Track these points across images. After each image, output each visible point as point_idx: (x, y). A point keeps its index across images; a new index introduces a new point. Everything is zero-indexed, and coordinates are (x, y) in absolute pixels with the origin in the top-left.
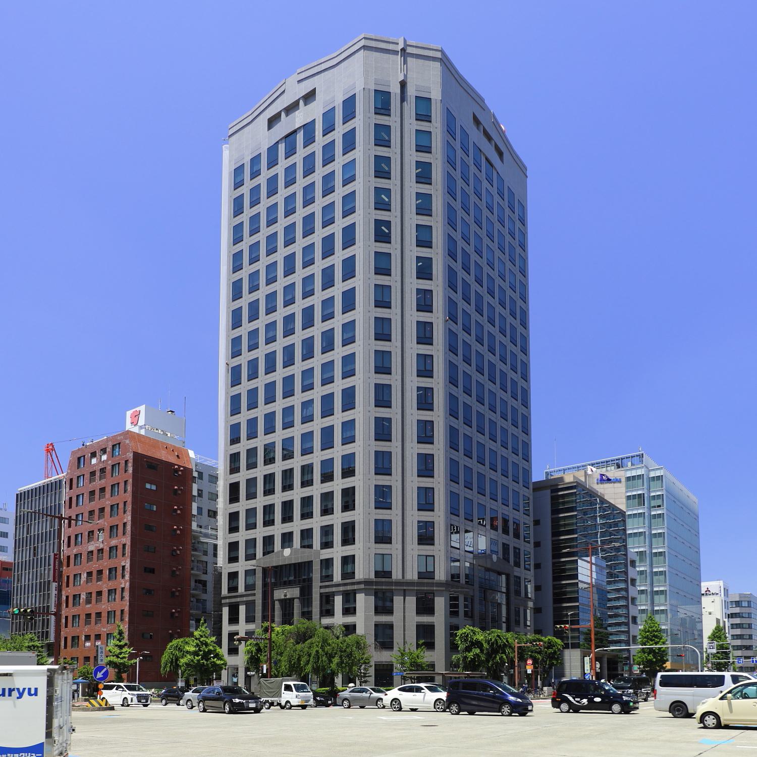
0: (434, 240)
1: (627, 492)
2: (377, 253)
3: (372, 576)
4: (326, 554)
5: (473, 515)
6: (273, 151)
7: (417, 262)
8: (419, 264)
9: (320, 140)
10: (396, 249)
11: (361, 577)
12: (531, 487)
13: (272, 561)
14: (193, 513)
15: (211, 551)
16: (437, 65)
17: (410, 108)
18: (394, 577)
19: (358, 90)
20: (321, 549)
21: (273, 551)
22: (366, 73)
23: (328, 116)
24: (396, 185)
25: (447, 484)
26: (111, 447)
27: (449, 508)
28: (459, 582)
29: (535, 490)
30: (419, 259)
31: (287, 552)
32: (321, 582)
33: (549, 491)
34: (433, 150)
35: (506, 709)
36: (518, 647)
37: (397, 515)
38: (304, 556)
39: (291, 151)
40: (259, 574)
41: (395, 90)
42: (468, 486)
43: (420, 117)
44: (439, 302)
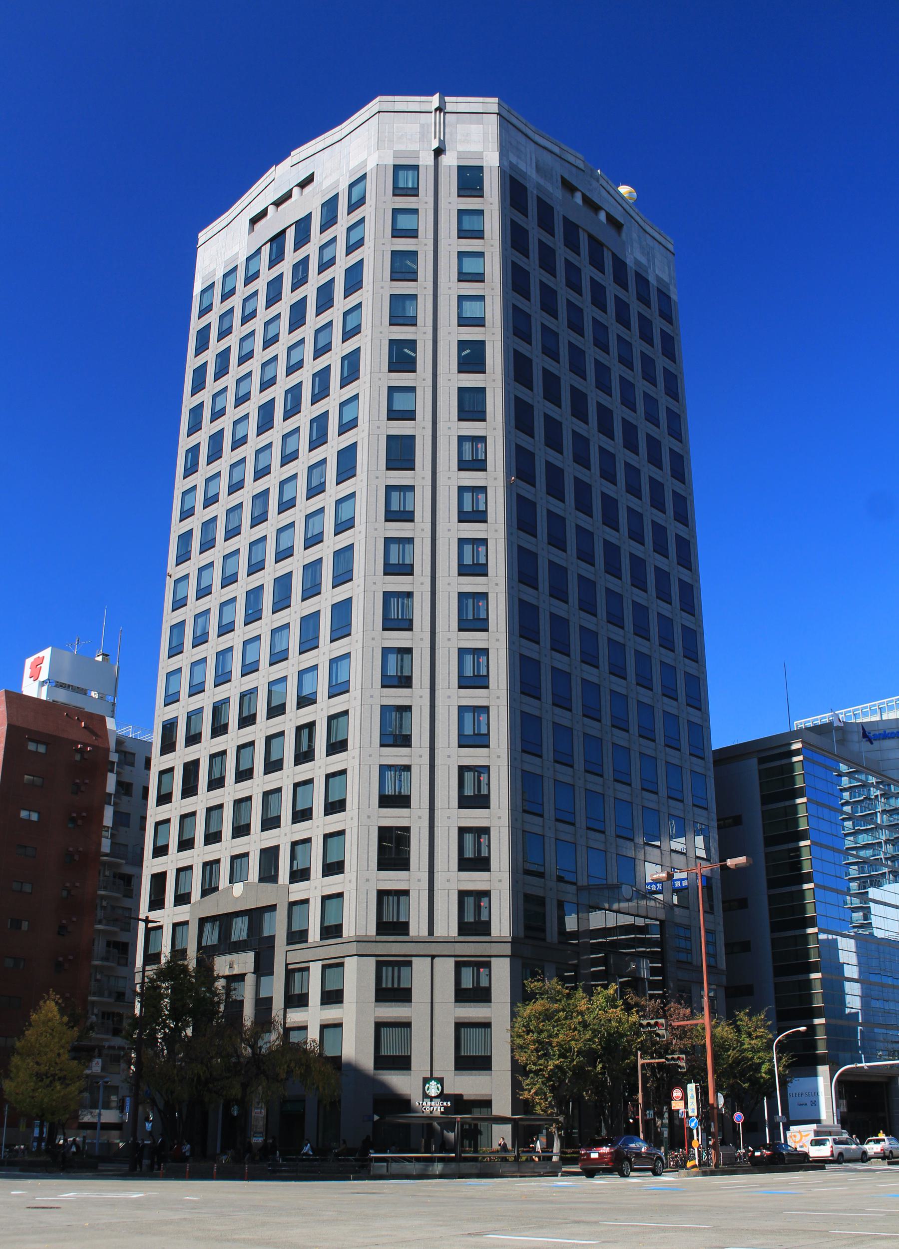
1: (110, 804)
2: (394, 253)
3: (372, 931)
4: (298, 891)
5: (574, 813)
7: (460, 350)
8: (464, 354)
9: (317, 238)
10: (424, 380)
11: (352, 934)
13: (215, 906)
15: (140, 762)
17: (449, 183)
18: (413, 931)
19: (371, 166)
20: (291, 883)
21: (216, 889)
23: (330, 207)
24: (425, 288)
25: (515, 759)
27: (518, 684)
28: (544, 940)
29: (716, 763)
30: (462, 345)
31: (238, 889)
32: (288, 944)
33: (754, 762)
34: (487, 234)
36: (643, 1065)
38: (265, 895)
39: (277, 258)
41: (426, 160)
42: (564, 759)
43: (466, 864)
44: (495, 357)
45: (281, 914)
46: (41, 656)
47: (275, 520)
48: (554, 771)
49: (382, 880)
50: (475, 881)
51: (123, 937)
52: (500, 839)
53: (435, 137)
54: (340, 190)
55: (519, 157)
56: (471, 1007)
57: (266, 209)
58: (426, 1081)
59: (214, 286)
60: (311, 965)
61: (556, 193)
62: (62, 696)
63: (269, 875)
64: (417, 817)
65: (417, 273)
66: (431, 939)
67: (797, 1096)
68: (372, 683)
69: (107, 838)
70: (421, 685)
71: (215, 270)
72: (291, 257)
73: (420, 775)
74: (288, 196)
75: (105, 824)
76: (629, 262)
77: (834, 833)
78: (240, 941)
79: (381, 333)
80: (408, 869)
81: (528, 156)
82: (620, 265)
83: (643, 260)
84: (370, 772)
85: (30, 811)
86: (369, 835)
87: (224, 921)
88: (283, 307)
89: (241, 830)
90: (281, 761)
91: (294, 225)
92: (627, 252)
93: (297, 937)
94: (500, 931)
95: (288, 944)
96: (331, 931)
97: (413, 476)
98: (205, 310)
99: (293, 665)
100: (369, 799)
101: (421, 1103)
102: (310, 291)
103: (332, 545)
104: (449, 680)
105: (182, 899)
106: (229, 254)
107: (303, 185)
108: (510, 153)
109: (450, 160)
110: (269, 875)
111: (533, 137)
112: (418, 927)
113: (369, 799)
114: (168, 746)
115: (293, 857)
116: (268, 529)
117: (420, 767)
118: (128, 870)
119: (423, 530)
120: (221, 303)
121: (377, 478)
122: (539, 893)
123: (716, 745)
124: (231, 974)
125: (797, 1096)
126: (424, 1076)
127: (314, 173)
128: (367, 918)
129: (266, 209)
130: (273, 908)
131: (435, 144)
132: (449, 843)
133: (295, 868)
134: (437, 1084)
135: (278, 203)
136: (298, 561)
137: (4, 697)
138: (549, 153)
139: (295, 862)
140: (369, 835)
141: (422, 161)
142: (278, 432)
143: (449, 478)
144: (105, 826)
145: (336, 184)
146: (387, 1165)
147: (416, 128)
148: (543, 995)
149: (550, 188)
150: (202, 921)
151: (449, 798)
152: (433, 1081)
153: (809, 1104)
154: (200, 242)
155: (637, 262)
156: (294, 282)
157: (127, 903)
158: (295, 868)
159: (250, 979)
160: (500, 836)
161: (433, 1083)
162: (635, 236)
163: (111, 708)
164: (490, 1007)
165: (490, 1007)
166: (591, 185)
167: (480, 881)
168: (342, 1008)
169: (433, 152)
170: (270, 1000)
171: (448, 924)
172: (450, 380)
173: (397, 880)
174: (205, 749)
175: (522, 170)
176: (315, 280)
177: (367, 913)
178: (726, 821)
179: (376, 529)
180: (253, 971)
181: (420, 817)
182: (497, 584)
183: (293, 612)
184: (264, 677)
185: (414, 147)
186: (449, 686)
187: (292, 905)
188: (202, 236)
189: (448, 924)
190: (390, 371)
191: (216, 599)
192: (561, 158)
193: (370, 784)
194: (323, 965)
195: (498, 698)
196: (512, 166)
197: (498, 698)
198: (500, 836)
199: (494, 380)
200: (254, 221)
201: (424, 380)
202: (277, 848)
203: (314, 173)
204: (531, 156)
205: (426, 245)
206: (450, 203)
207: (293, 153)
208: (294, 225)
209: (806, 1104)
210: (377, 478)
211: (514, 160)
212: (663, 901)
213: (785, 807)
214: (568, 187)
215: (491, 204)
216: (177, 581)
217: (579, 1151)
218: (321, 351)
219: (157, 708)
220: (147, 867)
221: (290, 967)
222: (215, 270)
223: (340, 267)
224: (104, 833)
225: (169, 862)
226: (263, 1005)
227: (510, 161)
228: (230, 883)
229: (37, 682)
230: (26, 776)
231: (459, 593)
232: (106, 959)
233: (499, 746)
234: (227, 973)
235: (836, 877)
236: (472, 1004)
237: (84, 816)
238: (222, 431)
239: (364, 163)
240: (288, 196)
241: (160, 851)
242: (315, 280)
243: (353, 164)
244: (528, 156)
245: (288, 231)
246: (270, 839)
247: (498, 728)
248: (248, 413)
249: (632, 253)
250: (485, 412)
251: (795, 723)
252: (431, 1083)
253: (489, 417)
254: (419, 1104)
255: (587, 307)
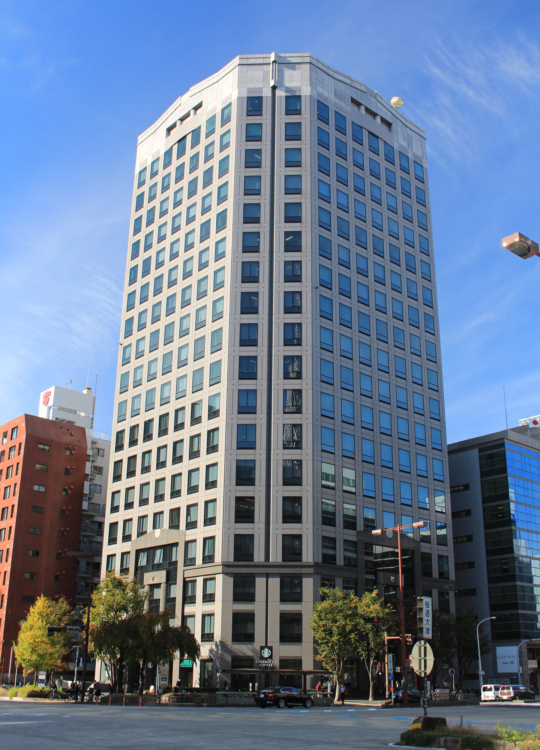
0: (303, 215)
1: (88, 481)
3: (320, 560)
4: (191, 535)
6: (168, 154)
7: (286, 237)
9: (204, 142)
10: (264, 227)
12: (446, 450)
14: (84, 493)
16: (308, 66)
17: (280, 107)
20: (186, 530)
21: (146, 532)
22: (240, 86)
23: (211, 121)
24: (266, 172)
26: (11, 430)
28: (335, 564)
31: (158, 532)
32: (184, 566)
33: (476, 452)
35: (282, 704)
36: (388, 640)
37: (260, 491)
38: (171, 537)
39: (181, 153)
40: (132, 557)
41: (267, 93)
45: (181, 547)
46: (49, 391)
47: (179, 313)
48: (342, 462)
49: (238, 529)
50: (293, 529)
51: (96, 560)
52: (307, 504)
53: (272, 79)
54: (217, 112)
55: (324, 88)
56: (290, 604)
57: (176, 123)
58: (262, 648)
59: (146, 169)
60: (217, 576)
61: (348, 109)
62: (63, 416)
63: (174, 525)
64: (258, 491)
65: (261, 162)
66: (267, 563)
67: (502, 658)
68: (232, 411)
69: (86, 501)
70: (261, 412)
71: (147, 159)
72: (189, 153)
73: (260, 466)
74: (187, 115)
75: (85, 492)
76: (396, 146)
77: (526, 495)
78: (508, 488)
79: (239, 200)
80: (253, 522)
81: (330, 87)
82: (389, 148)
83: (405, 145)
84: (231, 464)
85: (40, 485)
86: (230, 502)
87: (151, 551)
88: (184, 183)
89: (159, 498)
90: (181, 457)
91: (191, 133)
92: (394, 140)
93: (189, 562)
94: (307, 559)
95: (184, 566)
96: (208, 559)
97: (257, 286)
98: (141, 184)
99: (189, 400)
100: (230, 481)
101: (259, 661)
102: (199, 173)
103: (211, 328)
104: (278, 408)
105: (127, 538)
106: (155, 150)
107: (196, 109)
108: (318, 86)
109: (280, 93)
110: (174, 525)
111: (332, 75)
112: (259, 556)
113: (230, 481)
114: (119, 447)
115: (188, 514)
116: (175, 318)
117: (260, 461)
118: (98, 519)
119: (263, 319)
120: (150, 179)
121: (236, 288)
122: (332, 535)
123: (449, 443)
124: (153, 583)
125: (502, 658)
126: (261, 645)
127: (202, 101)
128: (228, 551)
129: (176, 123)
130: (176, 544)
131: (272, 83)
132: (277, 506)
133: (189, 521)
134: (269, 650)
135: (182, 120)
136: (192, 337)
137: (24, 418)
138: (343, 83)
139: (189, 517)
140: (230, 502)
141: (264, 94)
142: (181, 259)
143: (279, 287)
144: (85, 494)
145: (215, 108)
146: (226, 699)
147: (261, 73)
148: (330, 597)
149: (343, 105)
150: (138, 552)
151: (277, 479)
152: (266, 648)
153: (509, 663)
154: (139, 142)
155: (401, 146)
156: (191, 168)
157: (98, 539)
158: (189, 521)
159: (163, 586)
160: (307, 502)
161: (266, 649)
162: (399, 130)
163: (91, 421)
164: (301, 604)
165: (301, 604)
166: (371, 101)
167: (295, 529)
168: (214, 604)
169: (271, 89)
170: (174, 599)
171: (276, 554)
172: (280, 227)
173: (247, 529)
174: (140, 449)
175: (325, 96)
176: (203, 167)
177: (228, 548)
178: (460, 488)
179: (235, 319)
180: (165, 582)
181: (260, 491)
182: (307, 351)
183: (189, 368)
184: (172, 406)
185: (260, 85)
186: (278, 412)
187: (187, 543)
188: (140, 138)
189: (276, 554)
190: (244, 223)
191: (146, 359)
192: (351, 86)
193: (231, 471)
194: (204, 579)
195: (307, 419)
196: (319, 94)
197: (307, 419)
198: (307, 502)
199: (306, 227)
200: (169, 130)
201: (264, 227)
202: (179, 509)
203: (202, 101)
204: (331, 86)
205: (266, 145)
206: (281, 119)
207: (191, 89)
208: (191, 133)
209: (508, 663)
210: (236, 288)
211: (320, 90)
212: (413, 539)
213: (495, 479)
214: (356, 103)
215: (306, 119)
216: (125, 348)
217: (77, 685)
218: (205, 210)
219: (113, 424)
220: (107, 519)
221: (187, 579)
222: (147, 159)
223: (216, 159)
224: (84, 498)
225: (120, 516)
226: (170, 601)
227: (318, 91)
228: (153, 529)
229: (47, 407)
230: (37, 465)
231: (284, 356)
232: (86, 573)
233: (307, 448)
234: (151, 583)
235: (527, 522)
236: (290, 603)
237: (72, 488)
238: (150, 258)
239: (230, 96)
240: (187, 115)
241: (114, 509)
242: (203, 167)
243: (225, 96)
244: (330, 87)
245: (188, 136)
246: (175, 503)
247: (307, 437)
248: (165, 247)
249: (397, 141)
250: (301, 246)
251: (519, 421)
252: (265, 650)
253: (303, 249)
254: (258, 662)
255: (367, 177)
